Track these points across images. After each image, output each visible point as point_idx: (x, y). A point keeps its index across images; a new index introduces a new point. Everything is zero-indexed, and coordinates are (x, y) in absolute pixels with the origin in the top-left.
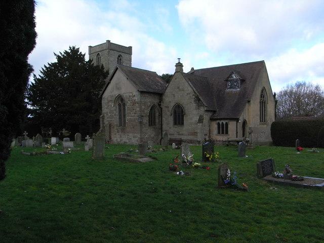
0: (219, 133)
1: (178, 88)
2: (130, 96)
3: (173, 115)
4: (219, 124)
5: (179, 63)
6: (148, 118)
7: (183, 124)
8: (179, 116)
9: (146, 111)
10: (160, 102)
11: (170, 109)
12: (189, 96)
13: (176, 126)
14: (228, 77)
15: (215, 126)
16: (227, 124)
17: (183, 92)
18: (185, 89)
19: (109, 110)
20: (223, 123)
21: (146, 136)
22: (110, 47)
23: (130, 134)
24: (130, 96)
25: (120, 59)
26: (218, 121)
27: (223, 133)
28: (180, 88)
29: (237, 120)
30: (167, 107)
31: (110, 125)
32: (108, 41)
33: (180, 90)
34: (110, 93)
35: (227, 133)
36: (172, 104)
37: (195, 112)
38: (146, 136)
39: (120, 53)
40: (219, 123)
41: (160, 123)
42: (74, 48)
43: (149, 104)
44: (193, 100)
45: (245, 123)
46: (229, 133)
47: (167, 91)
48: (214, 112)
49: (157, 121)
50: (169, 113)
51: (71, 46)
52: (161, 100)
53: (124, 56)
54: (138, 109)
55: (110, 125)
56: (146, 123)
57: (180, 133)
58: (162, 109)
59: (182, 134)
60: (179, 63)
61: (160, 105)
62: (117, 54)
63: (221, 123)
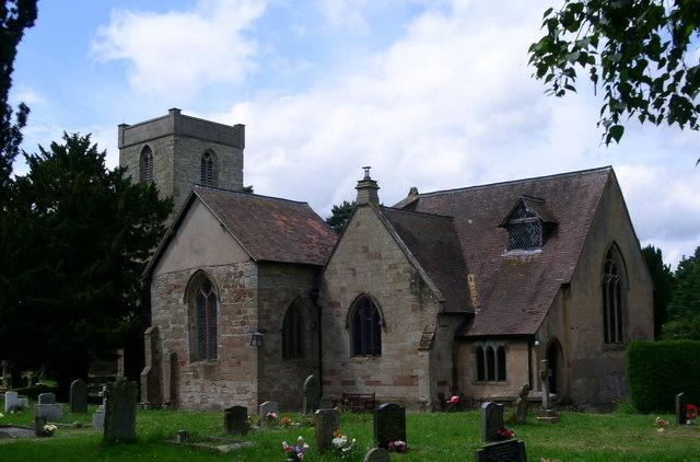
2: (229, 274)
4: (479, 352)
7: (378, 352)
8: (367, 325)
9: (274, 317)
10: (317, 290)
19: (169, 313)
20: (491, 348)
21: (275, 389)
25: (210, 162)
26: (477, 344)
27: (491, 378)
31: (174, 357)
33: (370, 257)
34: (180, 260)
36: (350, 297)
37: (412, 319)
44: (405, 286)
46: (509, 375)
49: (308, 343)
53: (222, 153)
55: (174, 357)
56: (276, 351)
57: (372, 379)
59: (378, 383)
60: (368, 179)
62: (202, 147)
63: (485, 349)
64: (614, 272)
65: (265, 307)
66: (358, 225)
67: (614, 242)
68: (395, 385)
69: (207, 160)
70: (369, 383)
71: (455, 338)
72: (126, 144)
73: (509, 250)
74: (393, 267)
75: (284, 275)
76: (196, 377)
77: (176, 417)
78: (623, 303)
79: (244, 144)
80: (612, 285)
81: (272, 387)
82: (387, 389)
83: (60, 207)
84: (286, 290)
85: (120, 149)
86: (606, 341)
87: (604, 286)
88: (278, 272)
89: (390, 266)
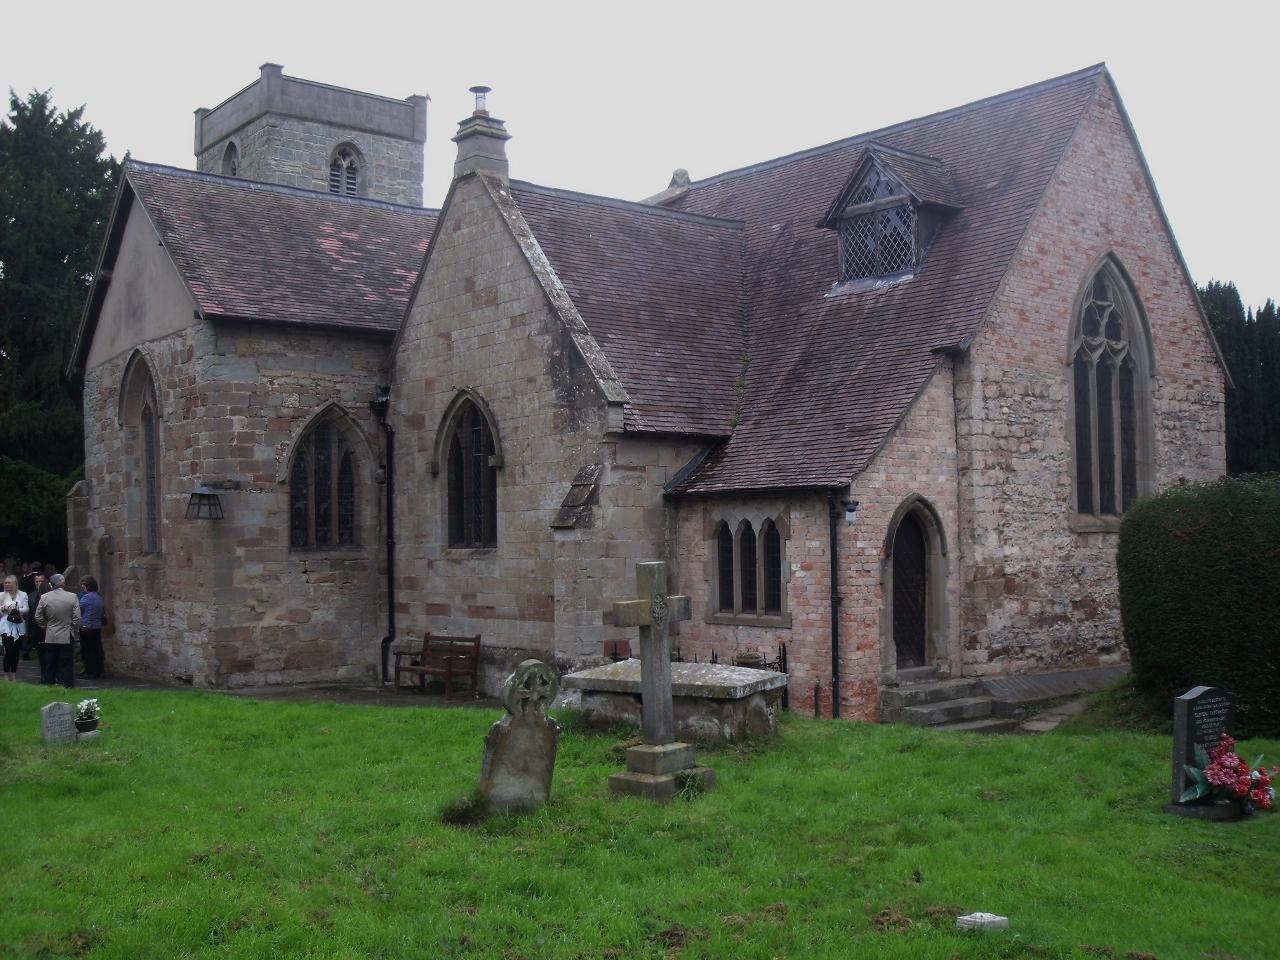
0: (726, 602)
1: (470, 284)
3: (443, 475)
4: (722, 533)
5: (481, 116)
6: (279, 500)
9: (261, 453)
10: (386, 391)
11: (432, 424)
12: (518, 333)
13: (460, 552)
14: (843, 200)
15: (698, 558)
16: (774, 536)
17: (489, 311)
18: (505, 289)
20: (747, 525)
21: (269, 620)
22: (279, 100)
23: (179, 606)
24: (174, 357)
25: (352, 169)
26: (717, 515)
27: (749, 604)
28: (480, 283)
29: (834, 501)
30: (416, 422)
32: (271, 70)
35: (774, 603)
36: (441, 401)
37: (553, 449)
38: (269, 620)
39: (348, 136)
40: (725, 525)
41: (384, 531)
42: (40, 101)
43: (293, 400)
44: (540, 364)
45: (913, 532)
46: (790, 603)
47: (419, 314)
48: (713, 447)
50: (421, 463)
51: (24, 99)
52: (388, 371)
54: (204, 440)
56: (268, 533)
58: (390, 435)
60: (481, 116)
61: (380, 410)
62: (326, 142)
64: (1114, 331)
65: (237, 429)
66: (457, 227)
67: (1111, 256)
68: (522, 617)
69: (345, 164)
70: (476, 612)
71: (667, 498)
72: (206, 144)
73: (841, 283)
74: (518, 321)
75: (291, 355)
76: (137, 590)
77: (668, 660)
78: (1138, 412)
79: (424, 134)
80: (1104, 368)
81: (260, 616)
82: (504, 626)
83: (84, 274)
84: (301, 390)
85: (196, 155)
86: (1085, 506)
87: (1080, 366)
88: (276, 346)
89: (513, 319)
